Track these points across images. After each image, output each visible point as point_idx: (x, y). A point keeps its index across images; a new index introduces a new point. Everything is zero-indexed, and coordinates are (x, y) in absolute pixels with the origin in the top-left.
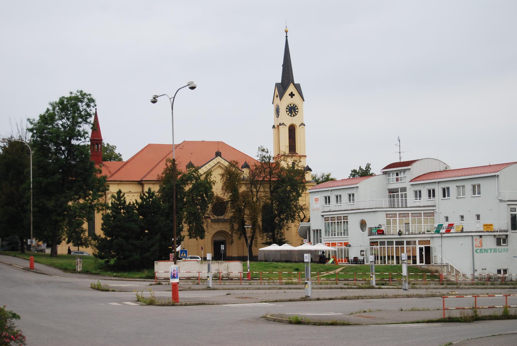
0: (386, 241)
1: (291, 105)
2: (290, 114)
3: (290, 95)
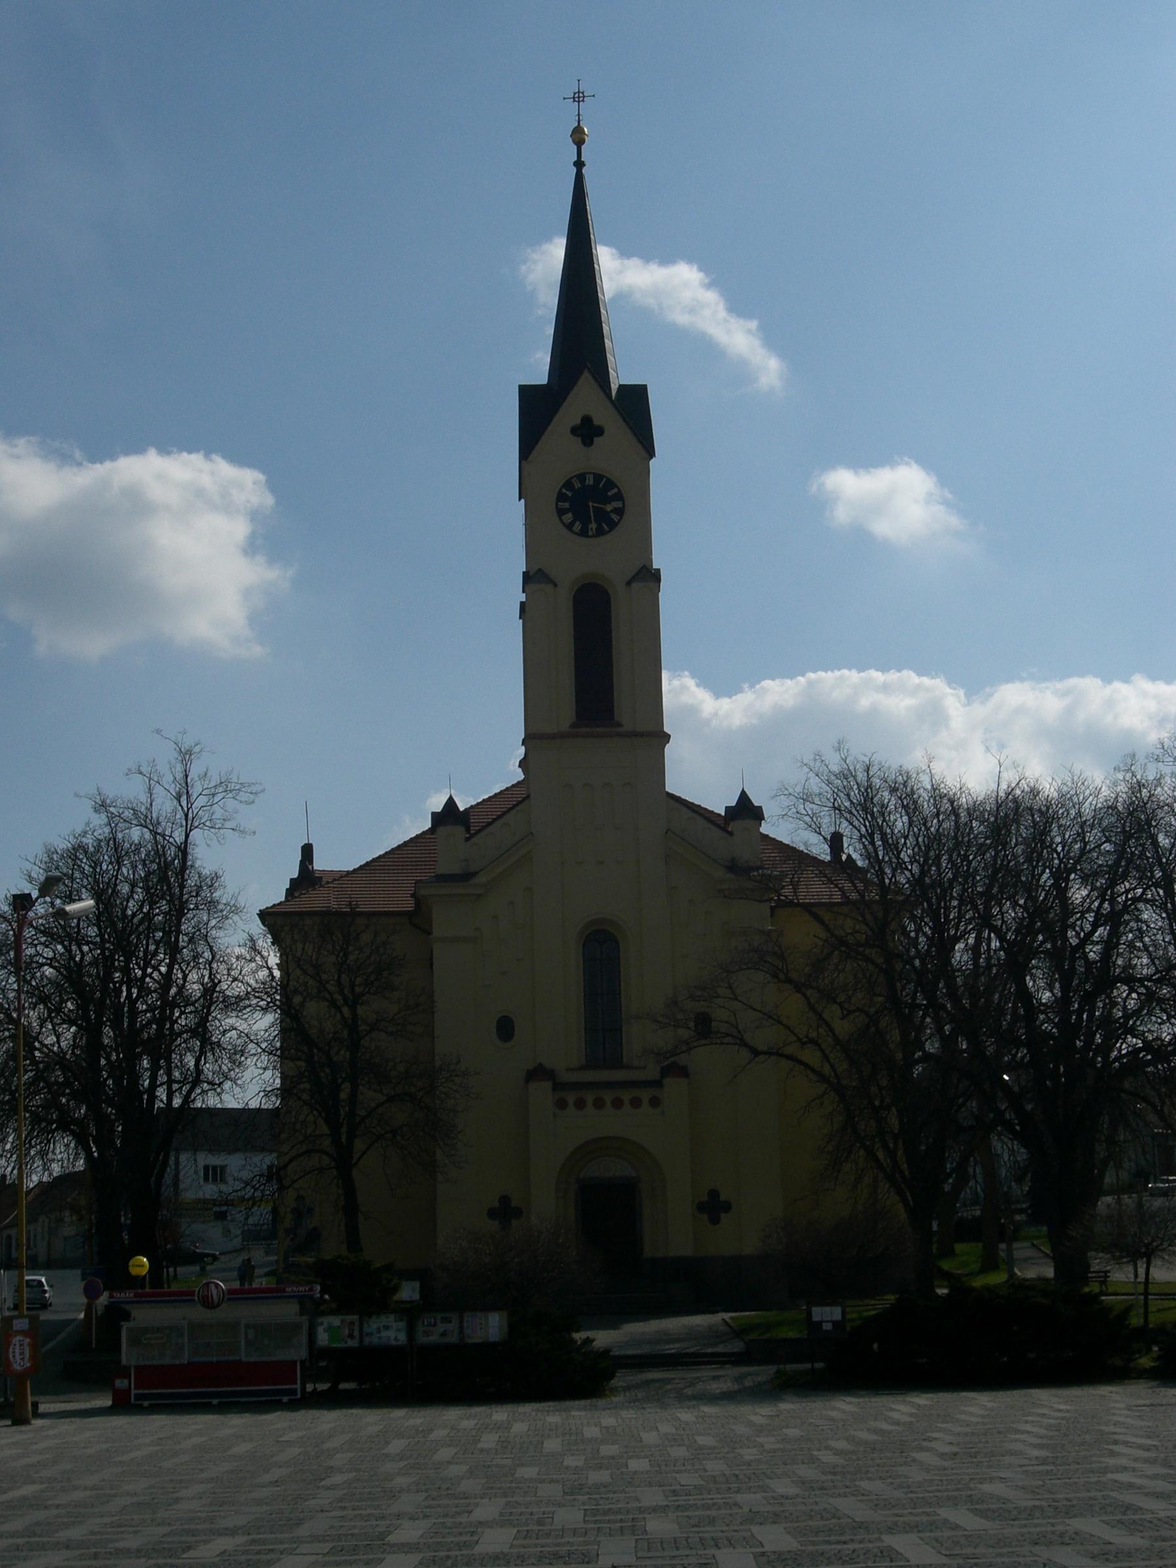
0: (147, 1290)
1: (569, 527)
2: (577, 527)
3: (574, 431)
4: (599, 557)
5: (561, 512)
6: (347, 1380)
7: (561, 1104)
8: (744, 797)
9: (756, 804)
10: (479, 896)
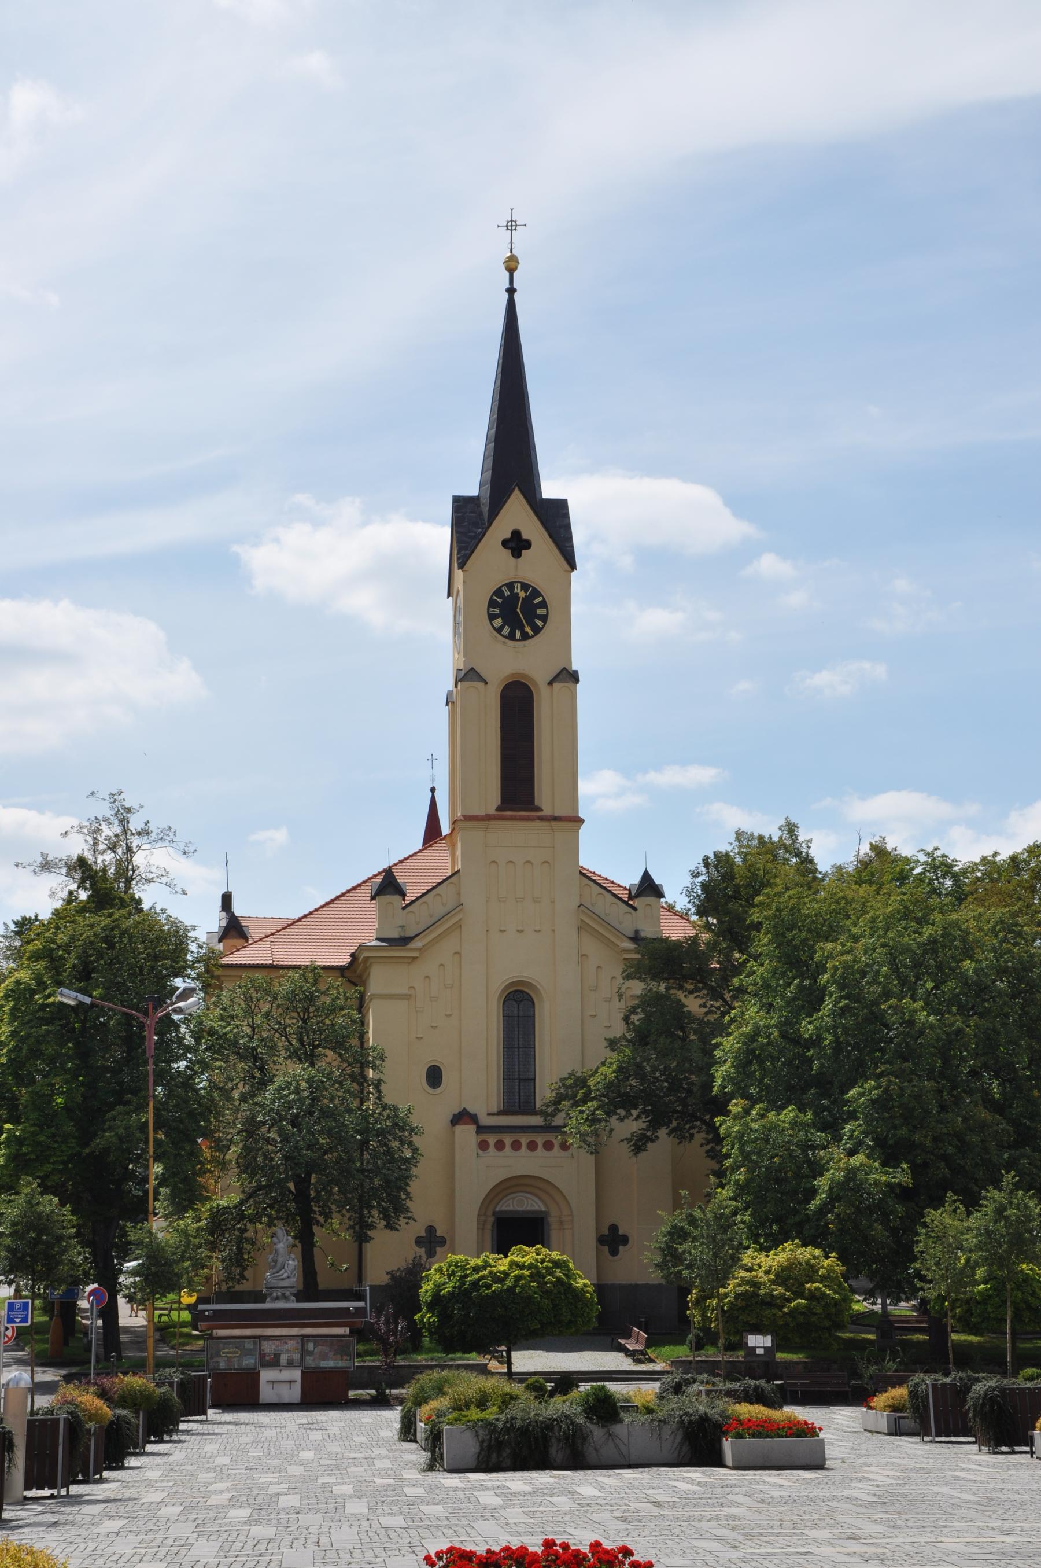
1: (499, 630)
2: (506, 631)
3: (505, 543)
4: (526, 660)
5: (492, 617)
6: (919, 1343)
7: (483, 1146)
8: (646, 876)
9: (657, 883)
10: (414, 958)
